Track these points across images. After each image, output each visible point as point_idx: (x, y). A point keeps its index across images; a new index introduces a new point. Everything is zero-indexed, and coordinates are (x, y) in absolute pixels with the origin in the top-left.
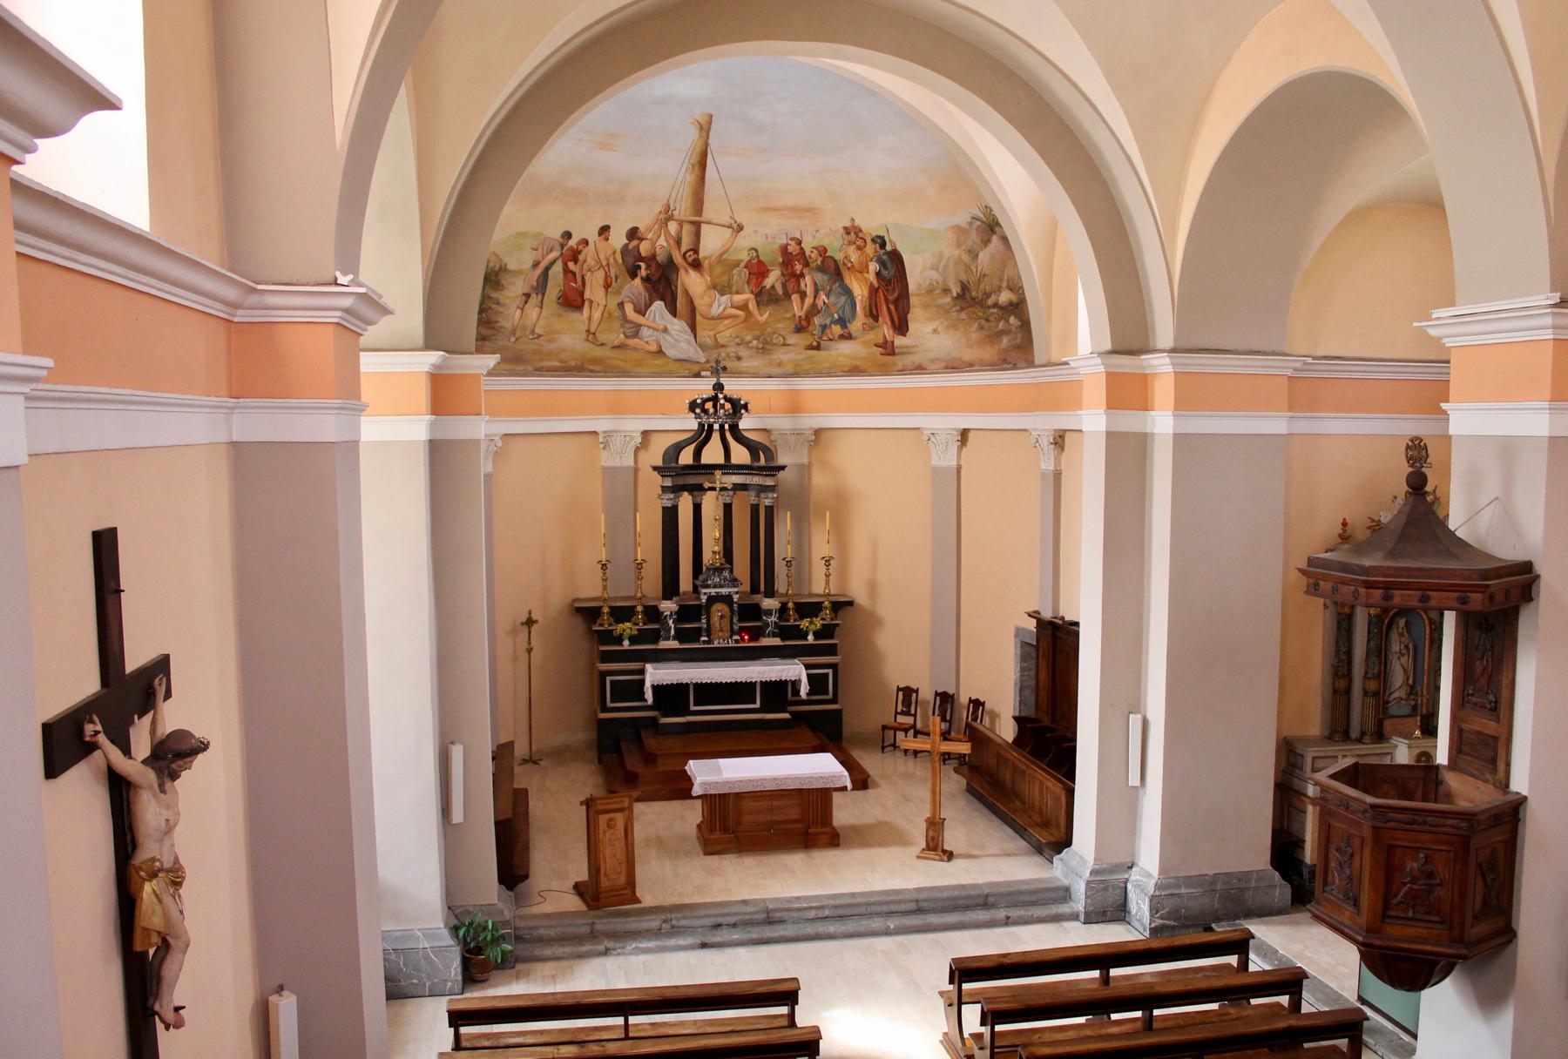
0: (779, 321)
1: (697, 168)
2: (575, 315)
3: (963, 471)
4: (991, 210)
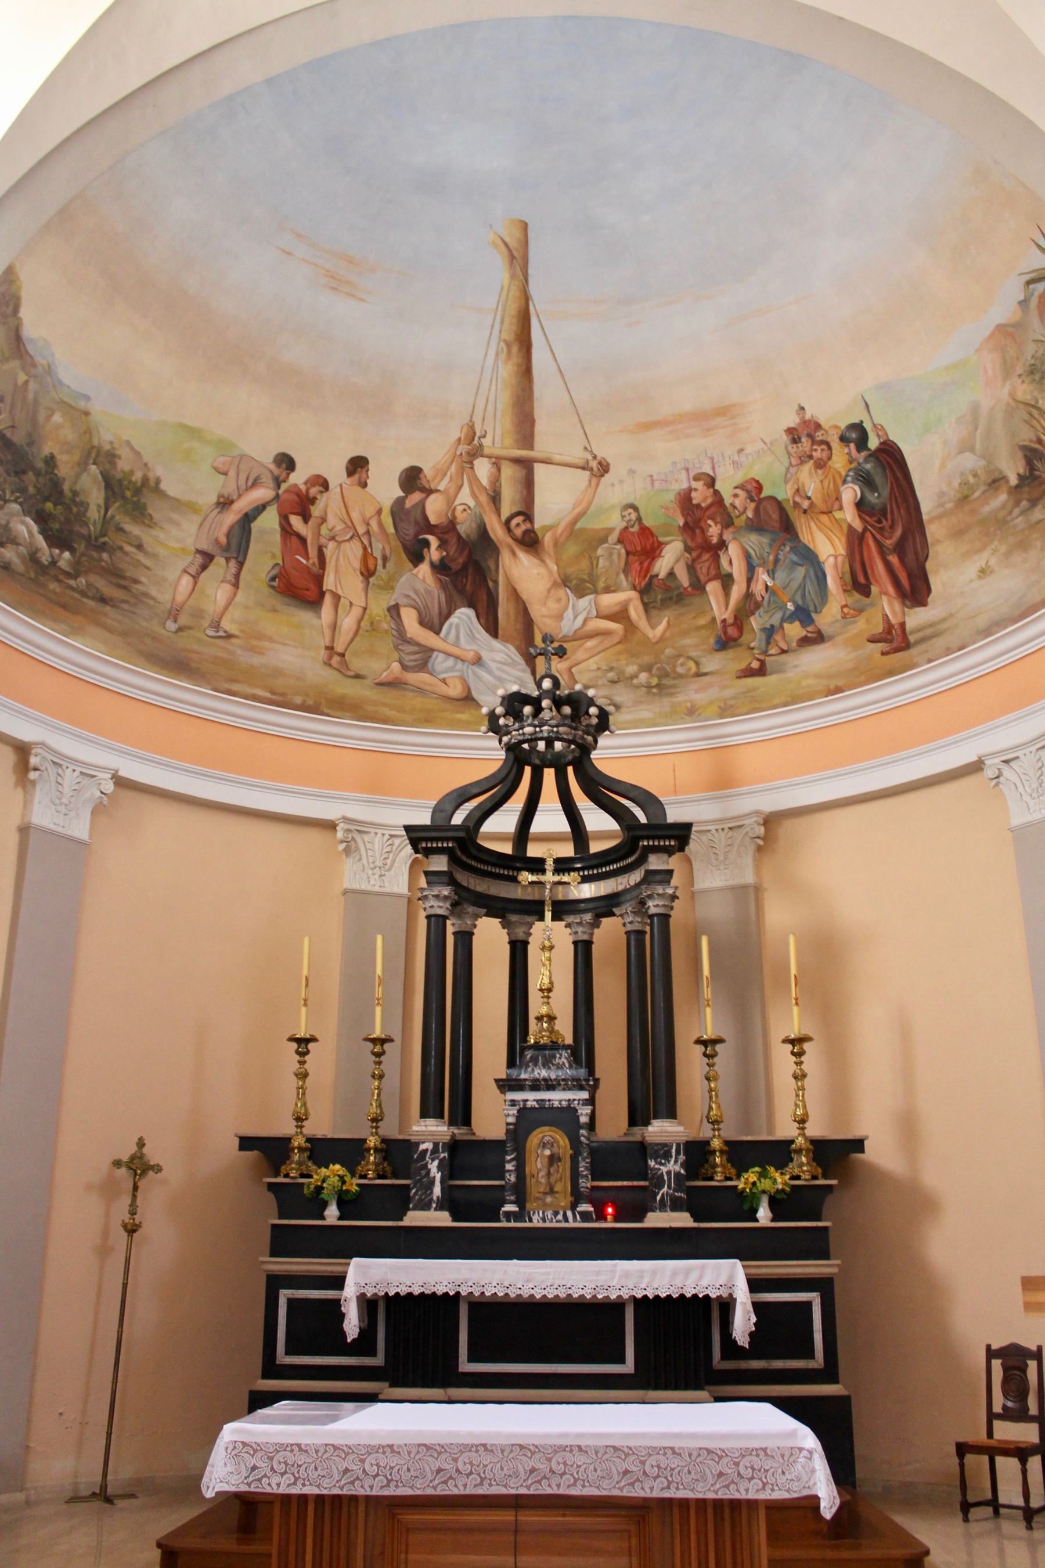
0: (685, 634)
1: (515, 349)
2: (305, 616)
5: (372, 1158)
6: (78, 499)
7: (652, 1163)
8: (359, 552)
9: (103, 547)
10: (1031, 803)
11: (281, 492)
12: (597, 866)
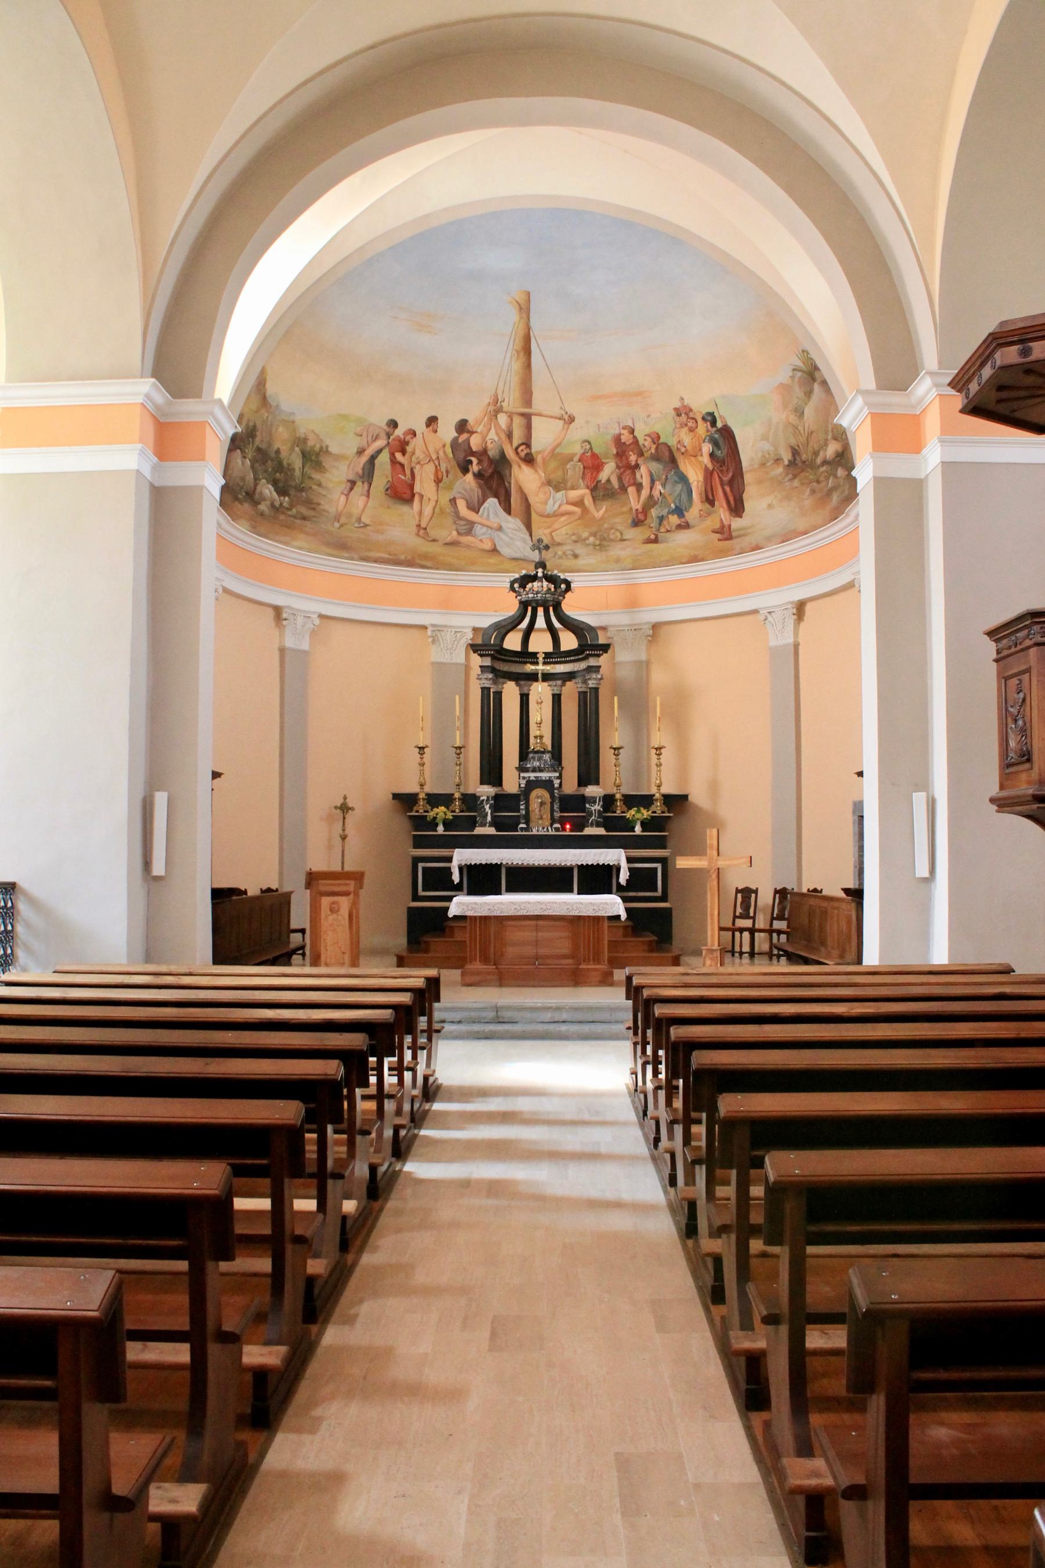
1: (522, 354)
2: (405, 509)
3: (800, 647)
4: (808, 353)
5: (457, 803)
6: (290, 468)
7: (587, 806)
8: (433, 469)
9: (302, 490)
10: (779, 635)
11: (390, 441)
12: (564, 657)
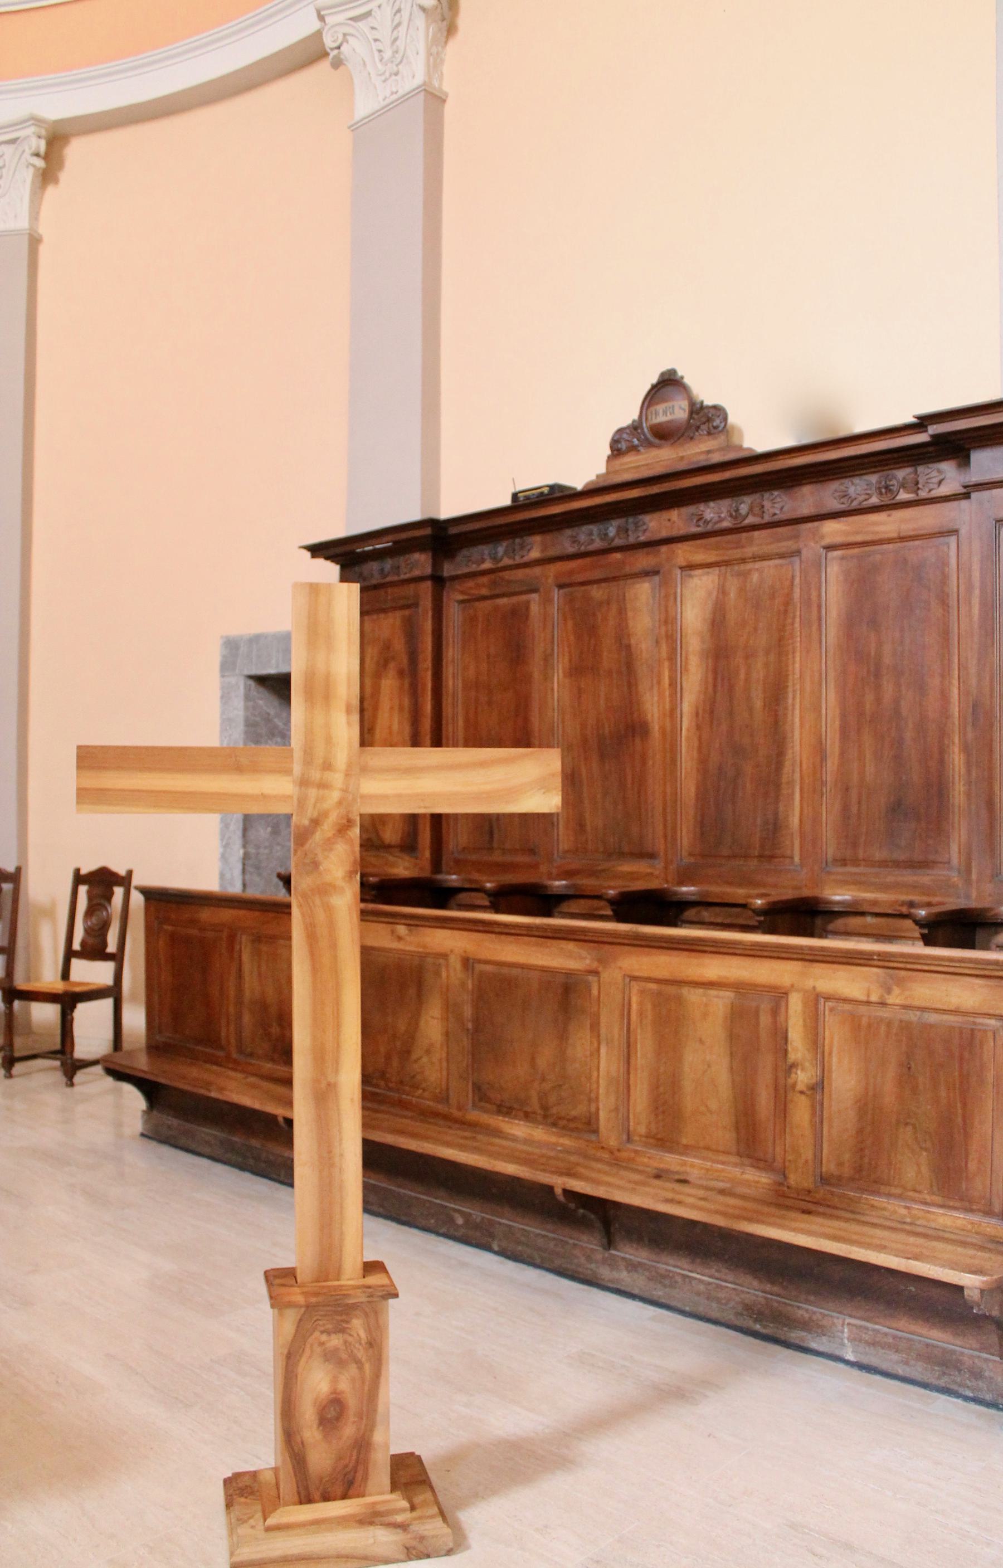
3: (43, 250)
